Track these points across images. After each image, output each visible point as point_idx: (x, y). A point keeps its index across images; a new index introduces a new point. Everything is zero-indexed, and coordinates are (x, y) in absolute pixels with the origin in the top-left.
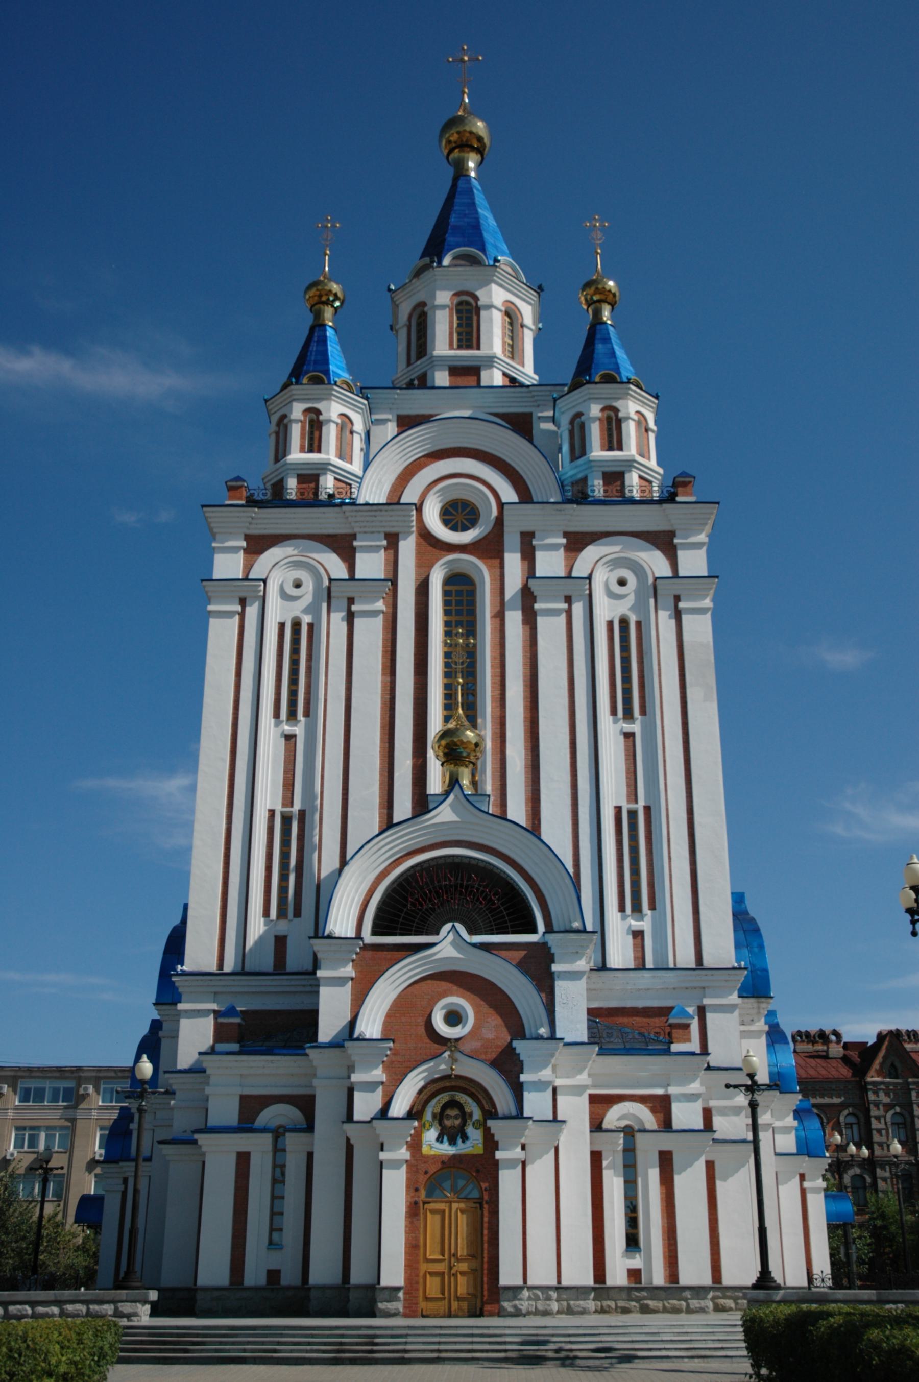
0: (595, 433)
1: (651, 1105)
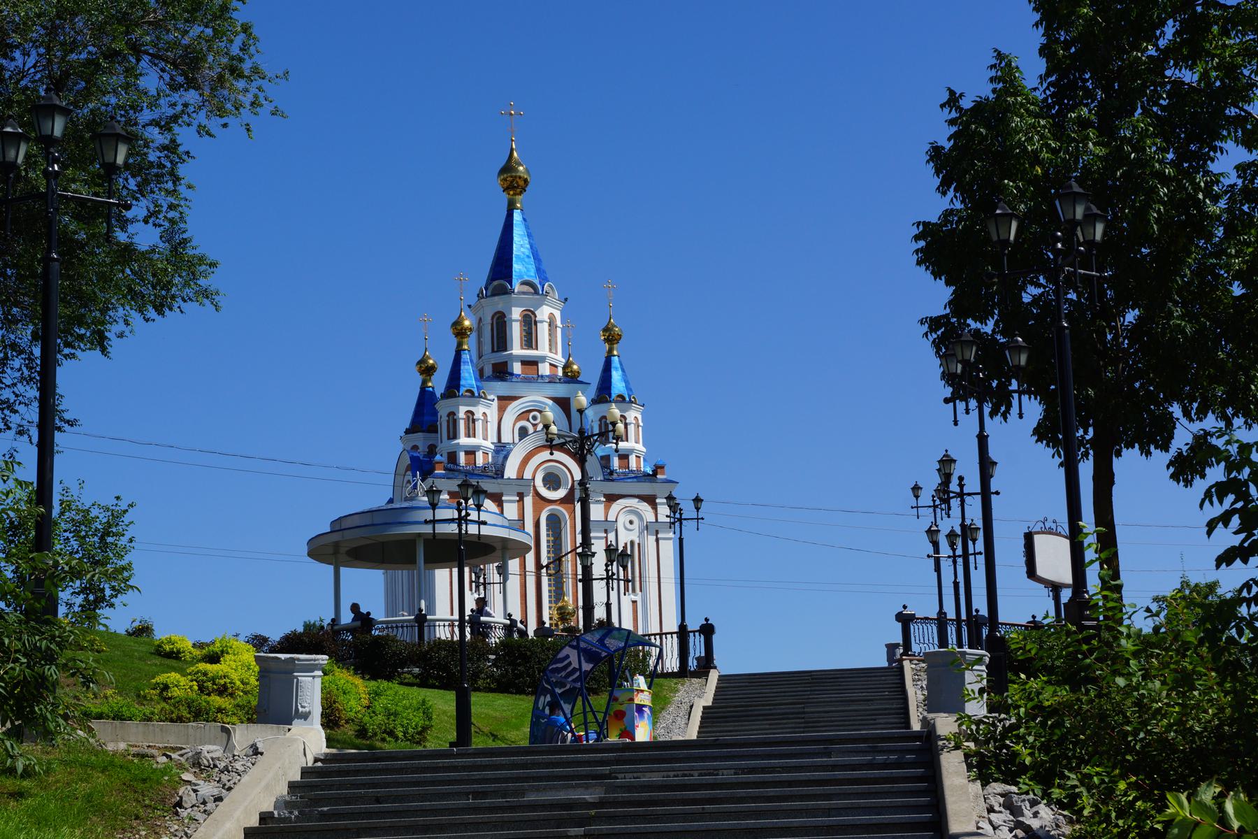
0: (516, 331)
1: (1080, 523)
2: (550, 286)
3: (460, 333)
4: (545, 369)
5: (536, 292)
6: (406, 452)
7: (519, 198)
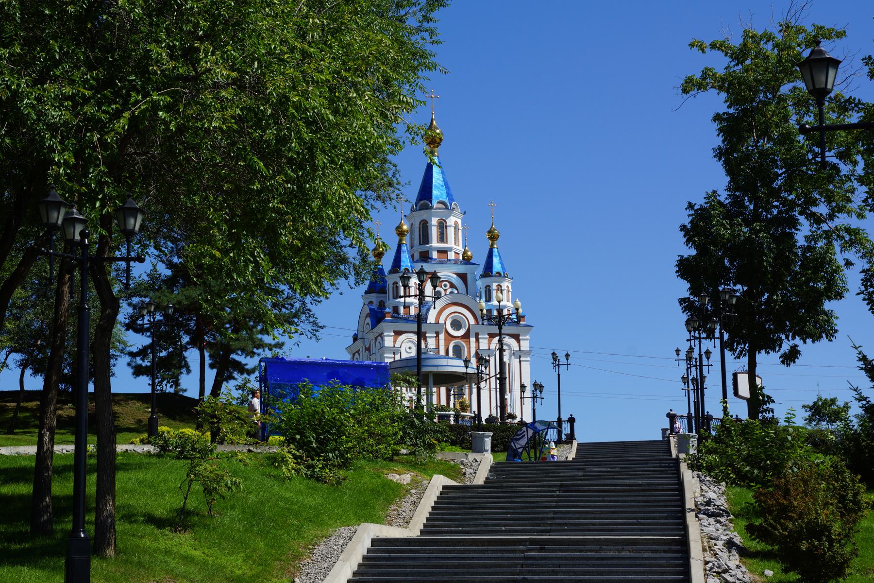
0: (434, 232)
2: (455, 204)
3: (401, 233)
4: (451, 256)
5: (447, 208)
6: (366, 306)
7: (436, 149)
